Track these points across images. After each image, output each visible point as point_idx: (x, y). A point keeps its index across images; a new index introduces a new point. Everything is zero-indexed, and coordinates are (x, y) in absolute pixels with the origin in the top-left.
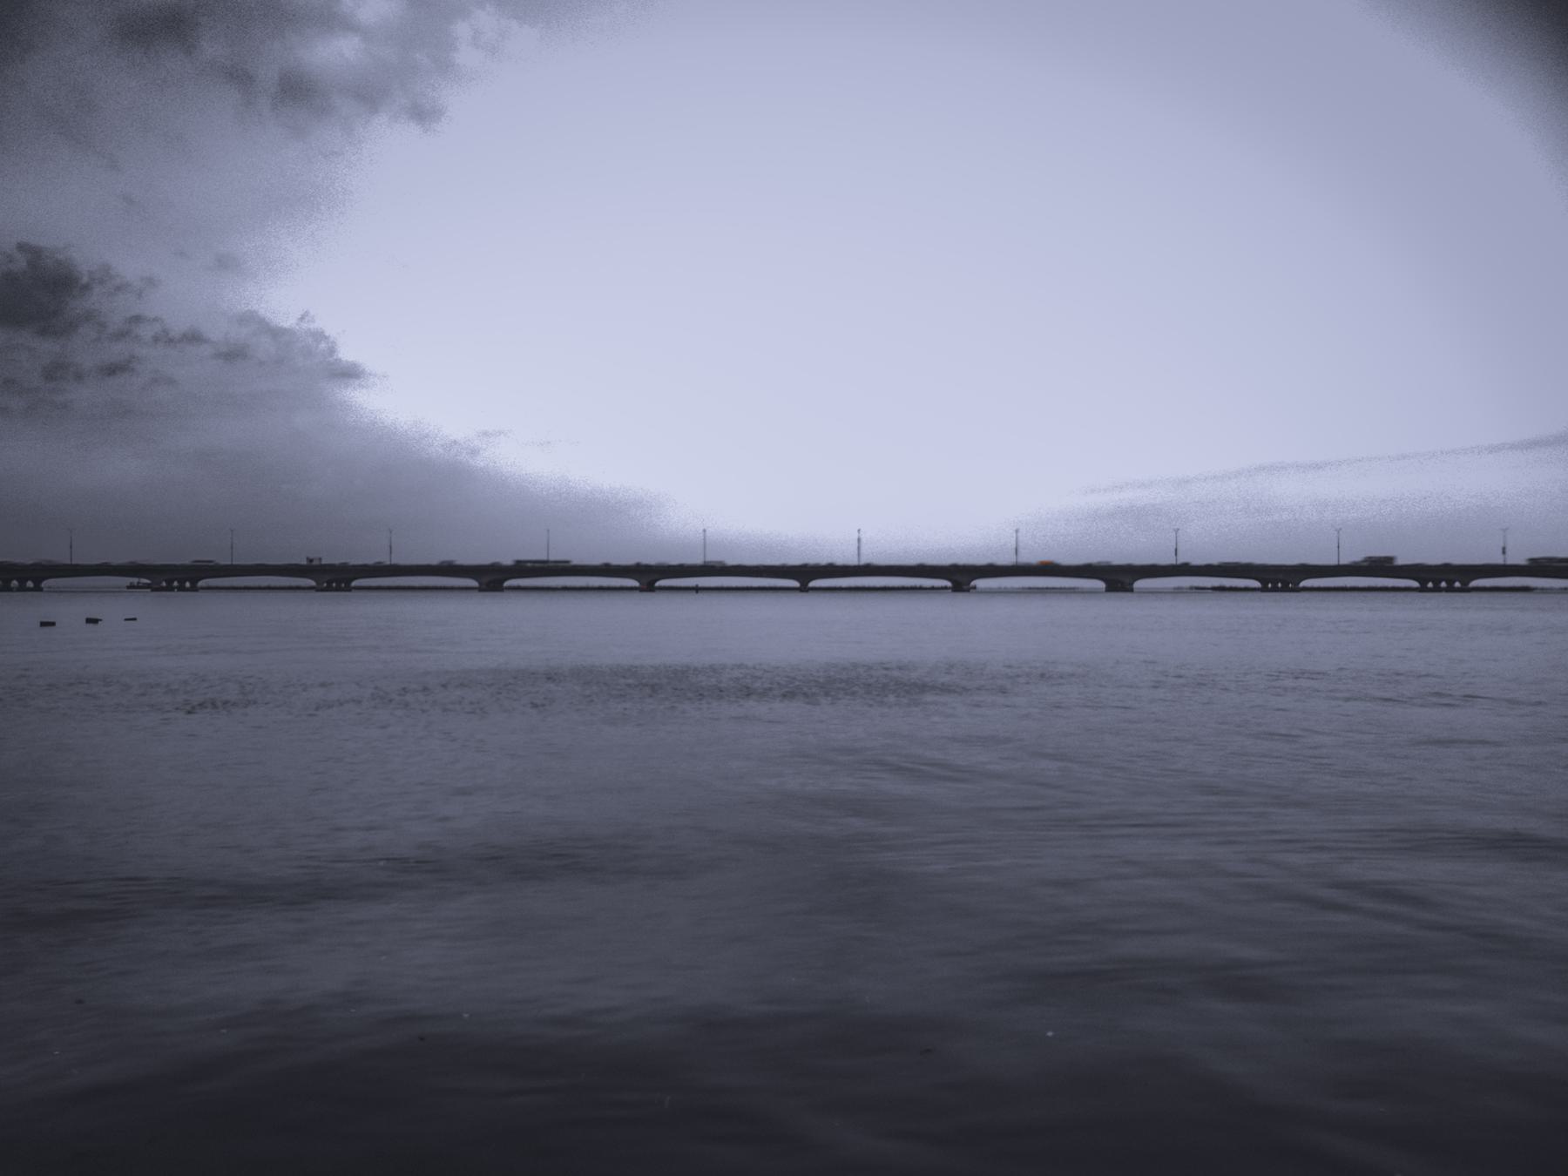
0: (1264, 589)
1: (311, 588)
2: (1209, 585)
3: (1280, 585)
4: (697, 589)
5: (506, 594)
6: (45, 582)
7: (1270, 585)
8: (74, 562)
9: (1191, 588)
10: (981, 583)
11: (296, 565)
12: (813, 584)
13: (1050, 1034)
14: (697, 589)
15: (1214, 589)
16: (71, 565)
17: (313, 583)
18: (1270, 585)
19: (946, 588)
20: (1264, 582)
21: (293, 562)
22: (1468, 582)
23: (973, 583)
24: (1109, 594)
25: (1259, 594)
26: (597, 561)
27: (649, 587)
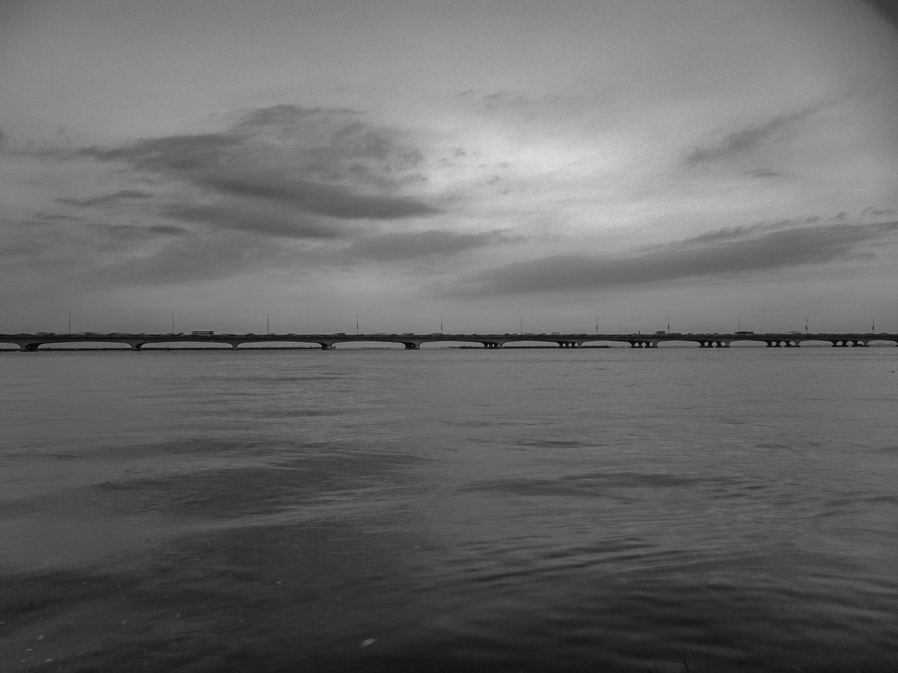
0: (486, 348)
1: (128, 349)
2: (102, 347)
3: (493, 345)
4: (168, 349)
5: (39, 352)
6: (848, 342)
7: (488, 346)
8: (598, 334)
9: (449, 347)
10: (338, 345)
11: (772, 334)
12: (239, 346)
13: (41, 637)
14: (810, 346)
15: (461, 348)
16: (597, 335)
17: (231, 346)
18: (488, 346)
19: (318, 348)
20: (486, 344)
21: (770, 332)
22: (867, 343)
23: (333, 345)
24: (408, 350)
25: (558, 349)
26: (105, 332)
27: (138, 348)
